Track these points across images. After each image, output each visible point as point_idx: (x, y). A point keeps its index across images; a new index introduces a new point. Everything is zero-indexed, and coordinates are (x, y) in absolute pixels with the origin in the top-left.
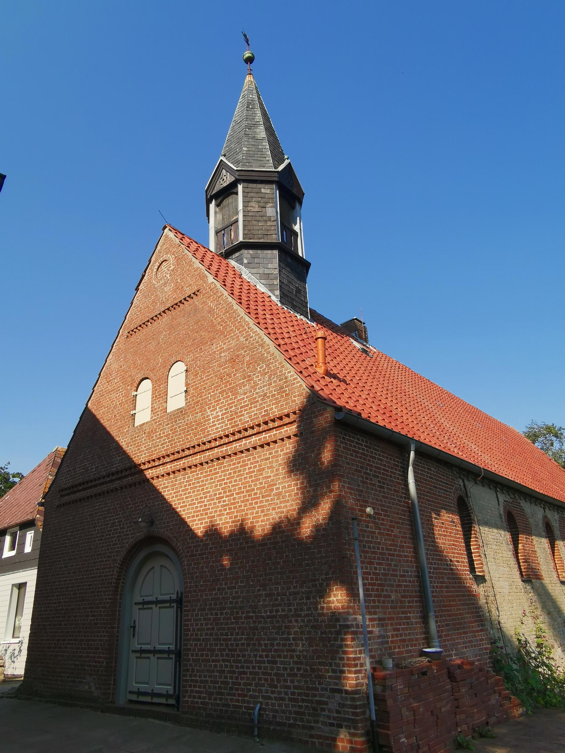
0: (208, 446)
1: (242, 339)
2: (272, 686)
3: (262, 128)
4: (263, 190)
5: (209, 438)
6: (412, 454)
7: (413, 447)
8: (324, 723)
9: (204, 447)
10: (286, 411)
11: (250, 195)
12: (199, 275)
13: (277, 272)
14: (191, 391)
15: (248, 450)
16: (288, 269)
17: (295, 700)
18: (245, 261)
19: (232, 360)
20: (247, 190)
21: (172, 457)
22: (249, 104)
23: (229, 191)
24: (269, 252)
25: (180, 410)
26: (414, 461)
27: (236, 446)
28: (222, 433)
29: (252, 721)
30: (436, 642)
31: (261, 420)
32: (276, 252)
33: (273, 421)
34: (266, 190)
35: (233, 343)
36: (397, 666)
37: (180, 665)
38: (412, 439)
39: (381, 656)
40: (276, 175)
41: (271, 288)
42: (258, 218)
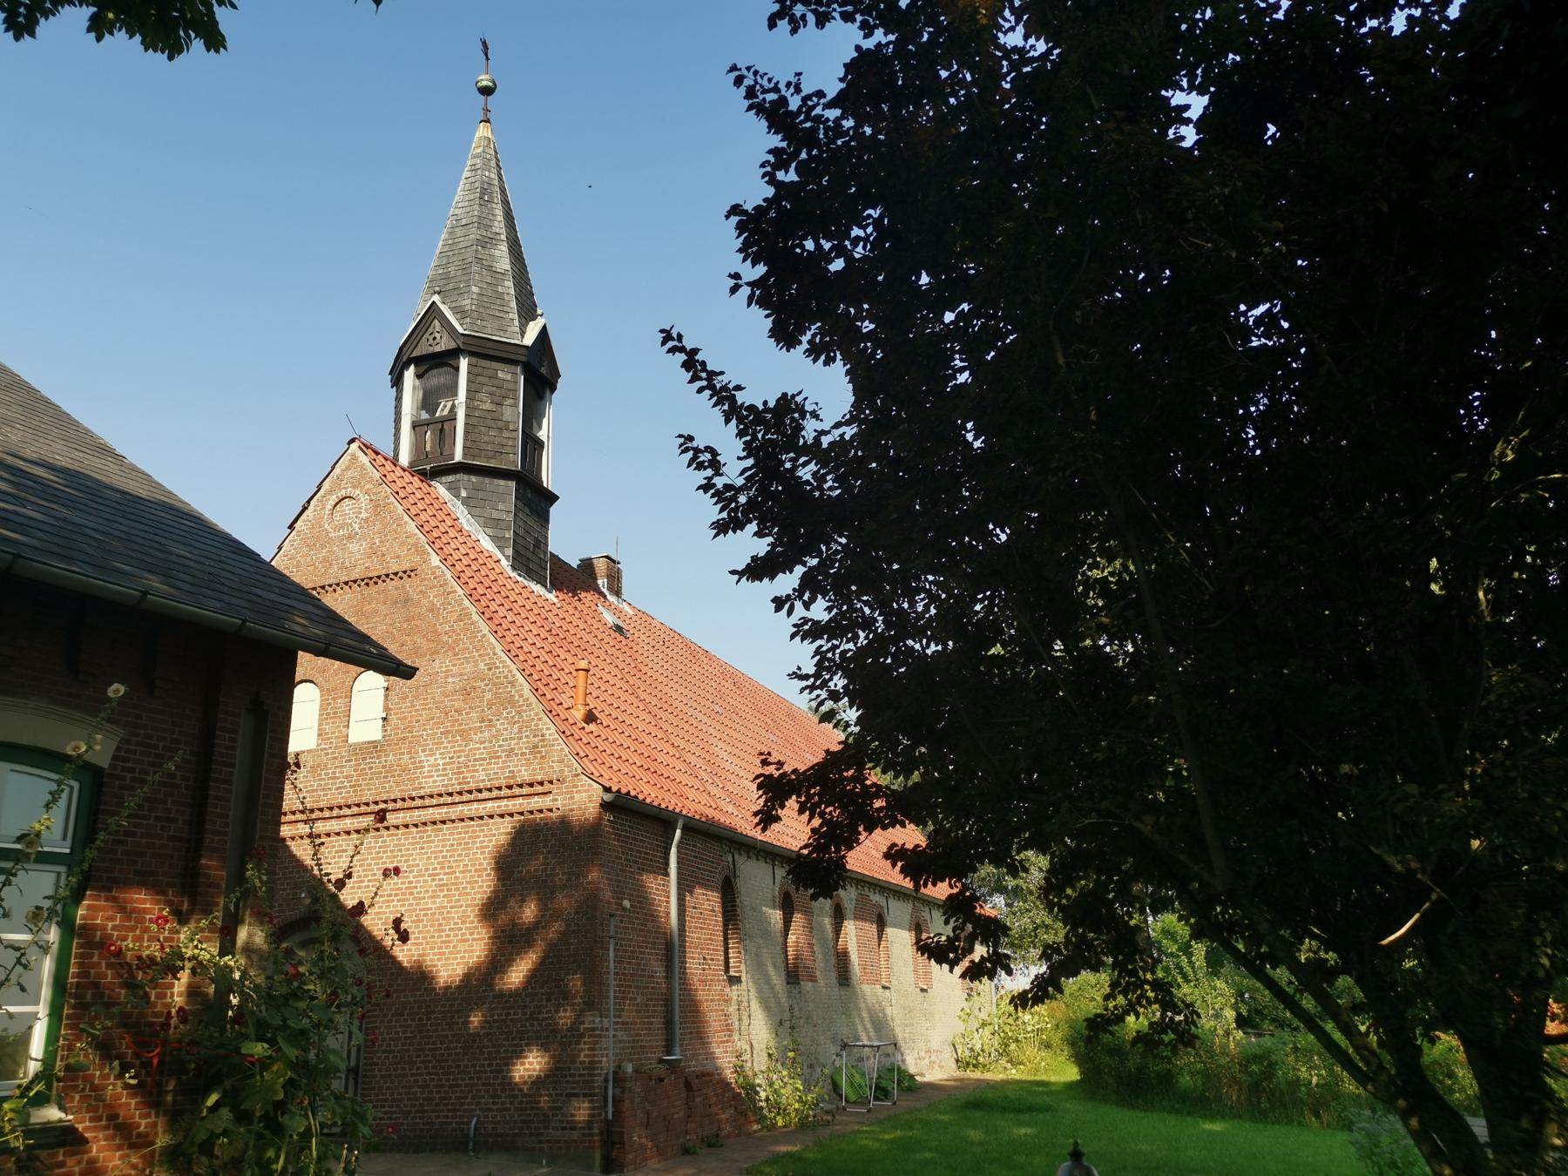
0: (418, 802)
1: (482, 666)
2: (493, 1097)
3: (504, 247)
4: (500, 375)
5: (422, 793)
6: (678, 832)
7: (680, 824)
8: (556, 1128)
9: (413, 804)
10: (539, 778)
11: (480, 379)
12: (416, 545)
13: (511, 517)
14: (393, 719)
15: (481, 818)
16: (527, 510)
17: (522, 1109)
18: (464, 494)
19: (466, 692)
20: (475, 370)
21: (355, 810)
22: (483, 191)
23: (445, 360)
24: (502, 482)
25: (374, 744)
26: (680, 842)
27: (465, 810)
28: (443, 790)
29: (467, 1136)
30: (677, 1049)
31: (503, 783)
32: (512, 484)
33: (521, 786)
34: (504, 373)
35: (468, 668)
36: (636, 1071)
37: (356, 1080)
38: (680, 814)
39: (621, 1061)
40: (524, 351)
41: (498, 541)
42: (489, 422)
